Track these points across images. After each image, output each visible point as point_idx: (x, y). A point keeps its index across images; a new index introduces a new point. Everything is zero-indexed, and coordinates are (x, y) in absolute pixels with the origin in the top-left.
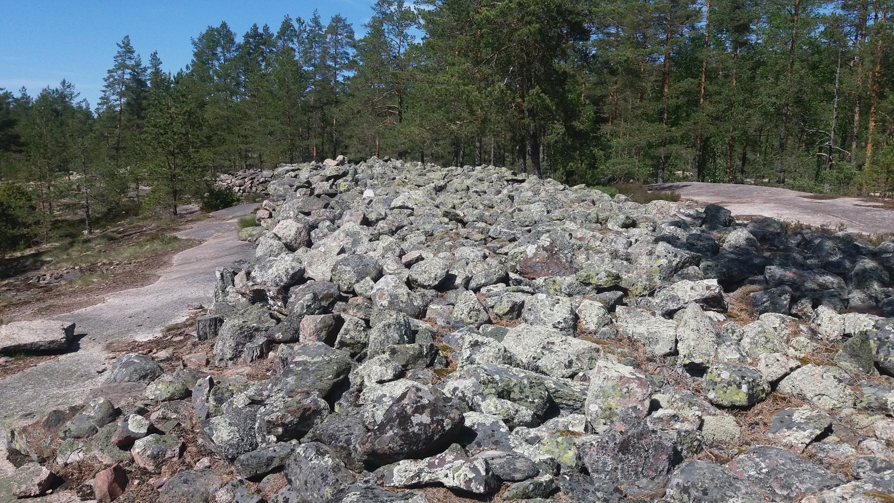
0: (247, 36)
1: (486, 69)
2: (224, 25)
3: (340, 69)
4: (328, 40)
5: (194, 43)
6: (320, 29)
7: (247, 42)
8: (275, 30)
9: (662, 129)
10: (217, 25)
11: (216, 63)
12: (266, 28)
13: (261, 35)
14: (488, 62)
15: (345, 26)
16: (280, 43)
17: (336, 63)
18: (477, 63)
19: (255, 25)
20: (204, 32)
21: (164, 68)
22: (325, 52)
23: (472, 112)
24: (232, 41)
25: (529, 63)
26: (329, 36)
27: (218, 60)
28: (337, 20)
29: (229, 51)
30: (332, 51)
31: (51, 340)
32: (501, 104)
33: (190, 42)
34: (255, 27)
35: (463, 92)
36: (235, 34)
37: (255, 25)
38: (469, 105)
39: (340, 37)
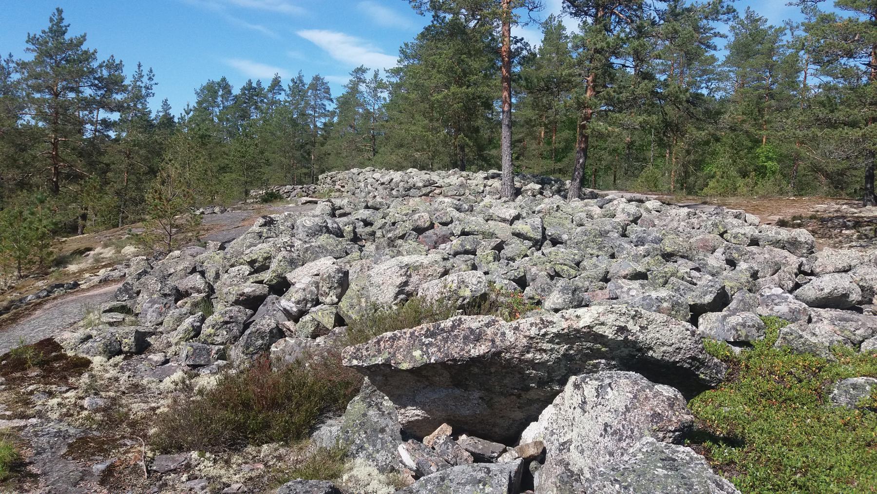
0: (244, 89)
1: (436, 124)
2: (224, 79)
3: (319, 117)
4: (309, 94)
5: (197, 93)
6: (303, 85)
7: (244, 94)
8: (266, 85)
9: (550, 164)
10: (218, 79)
11: (217, 110)
12: (259, 83)
13: (255, 88)
14: (437, 120)
15: (323, 84)
16: (270, 95)
17: (315, 111)
18: (431, 120)
19: (250, 81)
20: (205, 84)
21: (172, 112)
22: (307, 103)
23: (429, 147)
24: (230, 92)
25: (459, 122)
26: (310, 91)
27: (219, 107)
28: (317, 79)
29: (227, 101)
30: (313, 103)
31: (43, 338)
32: (445, 143)
33: (194, 92)
34: (250, 82)
35: (425, 136)
36: (233, 87)
37: (250, 81)
38: (428, 142)
39: (318, 92)
